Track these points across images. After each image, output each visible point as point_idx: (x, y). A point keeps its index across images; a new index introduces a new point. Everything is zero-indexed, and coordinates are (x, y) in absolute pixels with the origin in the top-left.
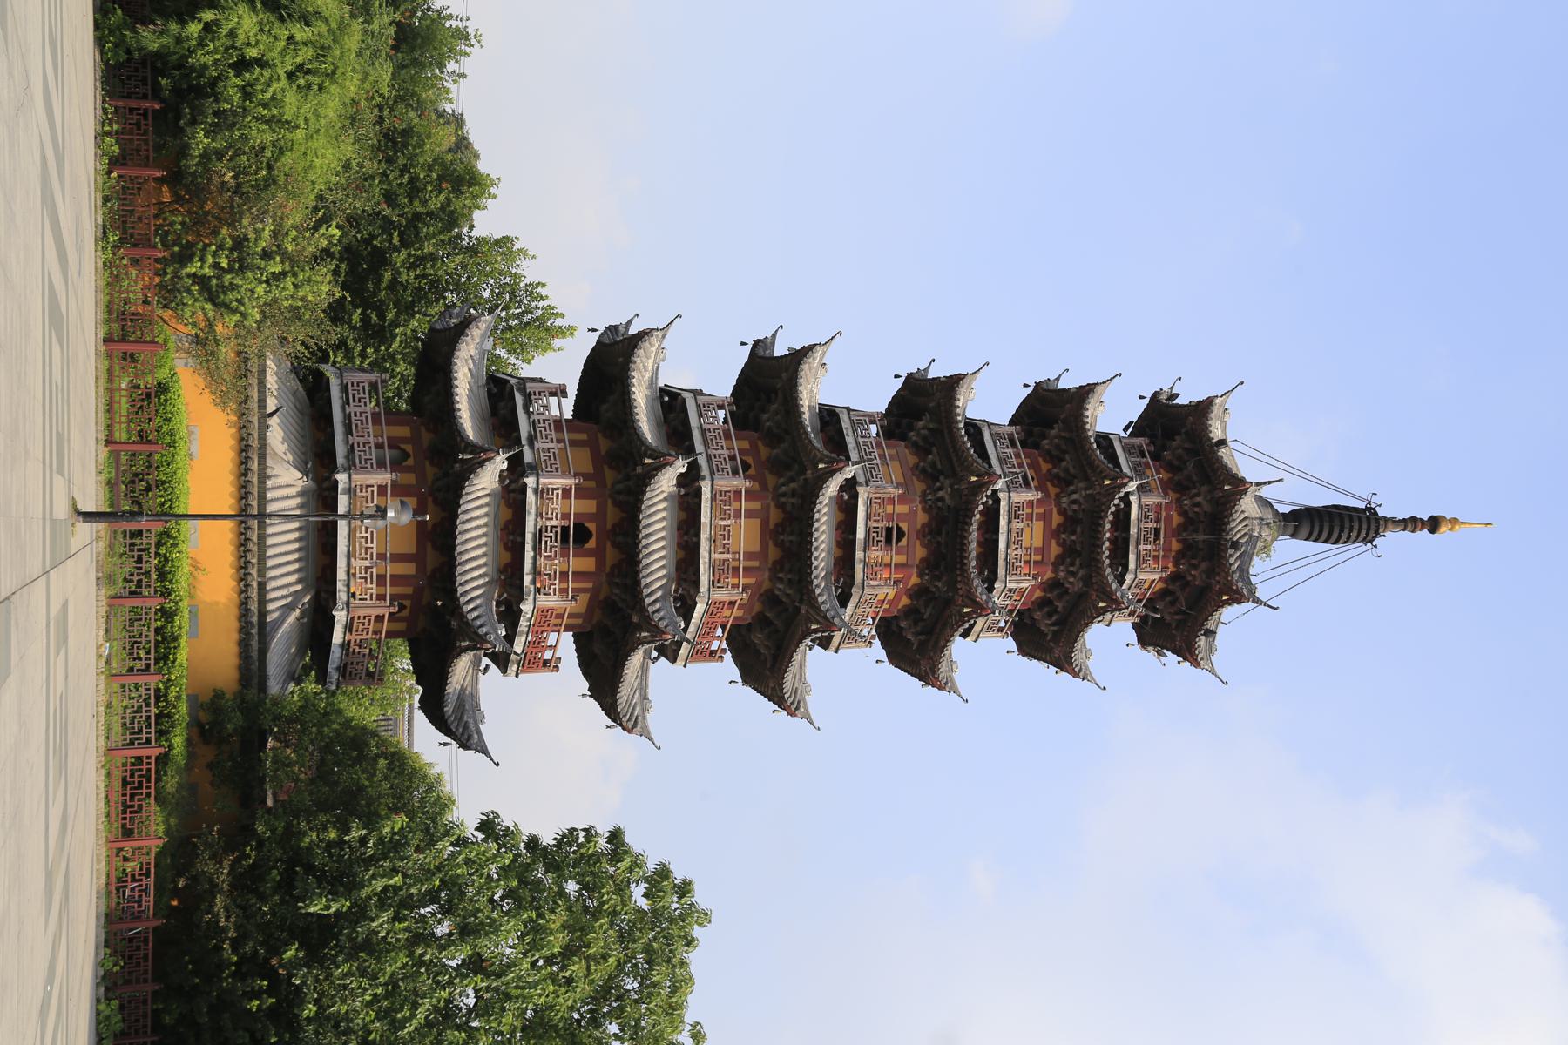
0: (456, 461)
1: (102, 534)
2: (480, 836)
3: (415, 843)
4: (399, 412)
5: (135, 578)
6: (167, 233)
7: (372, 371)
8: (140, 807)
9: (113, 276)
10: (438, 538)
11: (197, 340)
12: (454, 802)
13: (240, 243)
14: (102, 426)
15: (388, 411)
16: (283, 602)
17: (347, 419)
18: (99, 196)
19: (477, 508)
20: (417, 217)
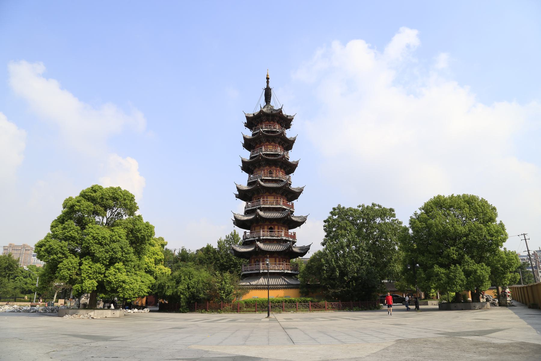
9: (226, 311)
11: (237, 297)
13: (220, 289)
17: (251, 270)
20: (214, 258)
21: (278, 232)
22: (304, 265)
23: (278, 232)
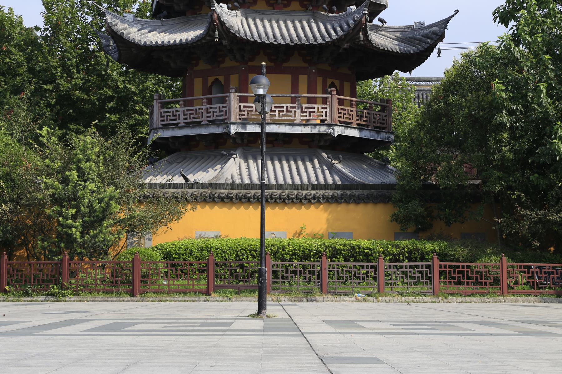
0: (220, 43)
1: (275, 298)
2: (512, 23)
3: (515, 74)
4: (183, 87)
5: (308, 275)
6: (50, 251)
7: (152, 106)
8: (477, 272)
9: (84, 290)
10: (280, 57)
11: (131, 231)
12: (485, 44)
13: (56, 200)
14: (195, 298)
15: (184, 95)
16: (327, 172)
17: (188, 125)
18: (24, 298)
19: (257, 27)
20: (31, 70)
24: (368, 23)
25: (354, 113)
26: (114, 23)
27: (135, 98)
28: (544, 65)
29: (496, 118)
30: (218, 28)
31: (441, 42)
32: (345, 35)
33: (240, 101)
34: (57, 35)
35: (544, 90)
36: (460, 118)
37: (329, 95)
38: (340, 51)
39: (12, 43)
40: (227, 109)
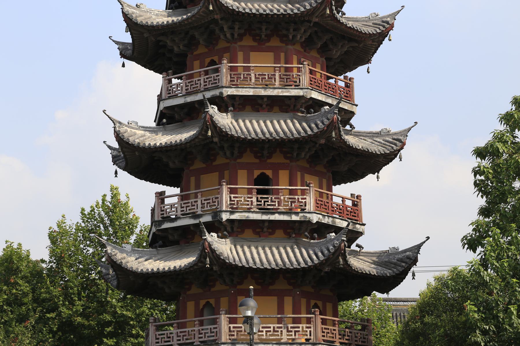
0: (211, 269)
2: (479, 249)
3: (485, 296)
4: (177, 310)
7: (148, 329)
10: (266, 281)
12: (455, 269)
15: (177, 318)
19: (244, 254)
20: (35, 300)
21: (292, 192)
22: (394, 328)
23: (292, 192)
24: (347, 249)
25: (337, 332)
26: (113, 254)
27: (131, 323)
28: (512, 288)
29: (471, 338)
30: (209, 255)
31: (415, 266)
32: (326, 260)
33: (230, 323)
34: (61, 266)
35: (515, 312)
36: (436, 337)
37: (313, 316)
38: (322, 274)
39: (20, 275)
40: (218, 330)
